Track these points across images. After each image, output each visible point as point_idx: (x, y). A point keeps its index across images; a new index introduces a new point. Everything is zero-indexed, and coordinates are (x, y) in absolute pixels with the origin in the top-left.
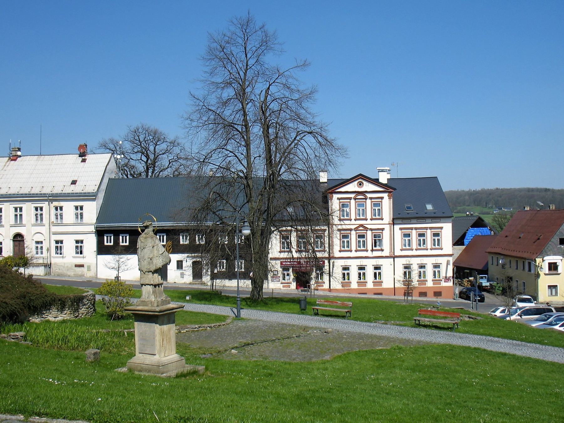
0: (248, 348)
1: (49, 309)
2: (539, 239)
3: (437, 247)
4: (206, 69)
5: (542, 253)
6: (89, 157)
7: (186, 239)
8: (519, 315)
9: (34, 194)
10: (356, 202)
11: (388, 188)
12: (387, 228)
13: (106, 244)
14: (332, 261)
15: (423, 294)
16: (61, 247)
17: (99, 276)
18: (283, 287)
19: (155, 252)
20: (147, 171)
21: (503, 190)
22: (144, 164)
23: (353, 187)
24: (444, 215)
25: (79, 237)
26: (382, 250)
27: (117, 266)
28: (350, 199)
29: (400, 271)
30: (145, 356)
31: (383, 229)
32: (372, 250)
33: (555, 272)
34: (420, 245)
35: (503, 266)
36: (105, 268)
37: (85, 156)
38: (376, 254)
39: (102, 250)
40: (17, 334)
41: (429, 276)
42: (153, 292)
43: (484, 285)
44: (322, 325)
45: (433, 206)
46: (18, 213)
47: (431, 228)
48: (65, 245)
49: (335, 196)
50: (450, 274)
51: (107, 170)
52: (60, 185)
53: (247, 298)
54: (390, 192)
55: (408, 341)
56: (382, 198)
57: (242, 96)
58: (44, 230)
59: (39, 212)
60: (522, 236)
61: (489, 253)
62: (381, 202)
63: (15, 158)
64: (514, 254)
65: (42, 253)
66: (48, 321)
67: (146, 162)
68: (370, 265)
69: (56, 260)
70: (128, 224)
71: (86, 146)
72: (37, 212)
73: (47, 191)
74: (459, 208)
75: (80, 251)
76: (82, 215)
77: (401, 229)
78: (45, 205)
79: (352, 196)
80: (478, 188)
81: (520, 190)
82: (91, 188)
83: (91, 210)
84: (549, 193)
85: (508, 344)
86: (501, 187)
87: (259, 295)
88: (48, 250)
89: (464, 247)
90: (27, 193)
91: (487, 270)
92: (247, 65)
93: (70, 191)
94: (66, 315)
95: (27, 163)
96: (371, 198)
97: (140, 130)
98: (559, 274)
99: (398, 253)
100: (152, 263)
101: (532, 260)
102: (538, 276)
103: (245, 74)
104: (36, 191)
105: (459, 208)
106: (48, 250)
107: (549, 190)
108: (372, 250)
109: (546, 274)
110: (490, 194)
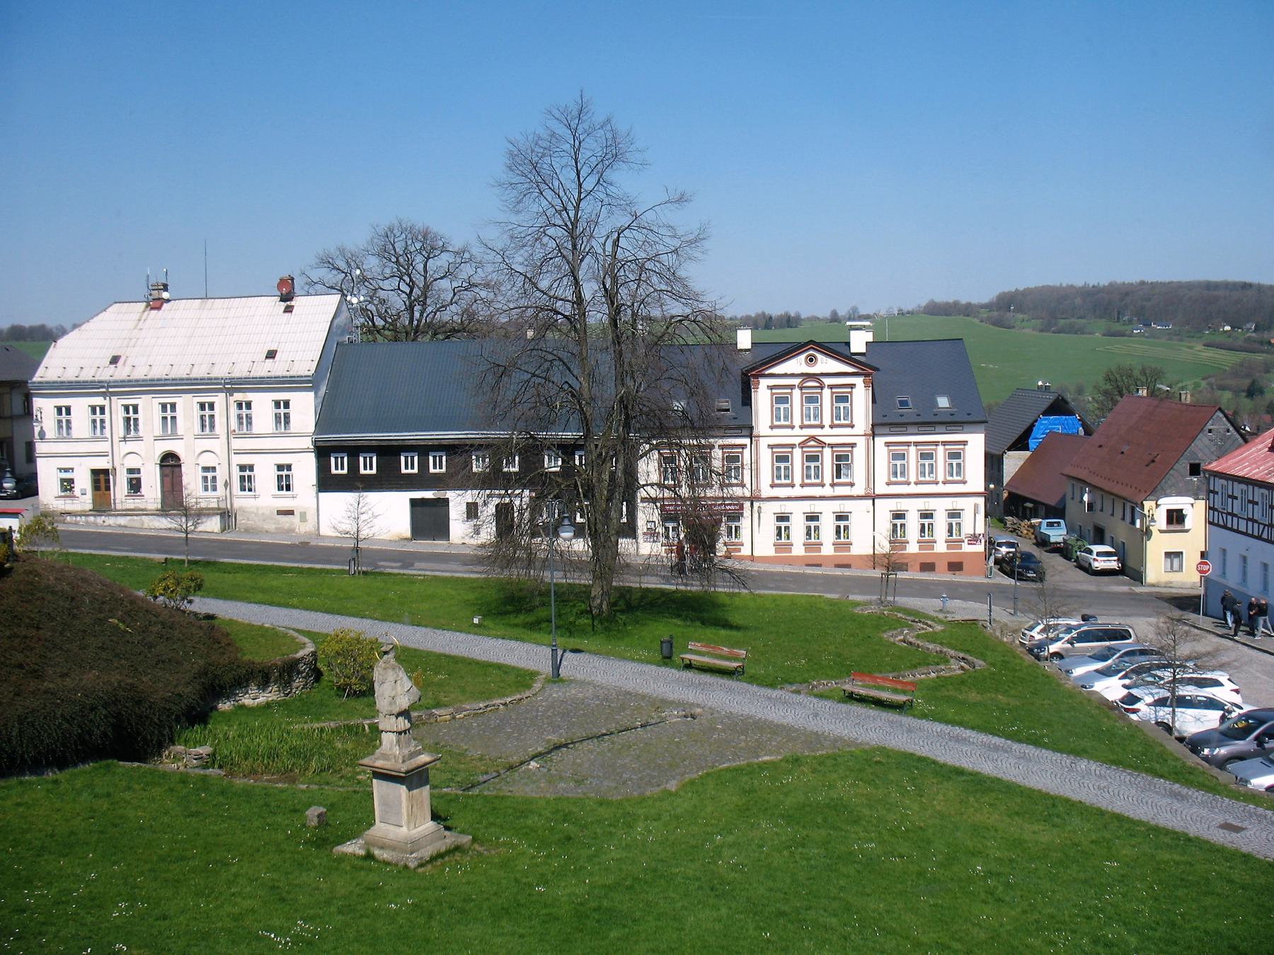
0: (556, 756)
5: (1155, 492)
6: (297, 302)
10: (802, 394)
11: (863, 365)
12: (861, 442)
13: (334, 471)
14: (756, 505)
15: (928, 567)
16: (250, 477)
17: (326, 531)
20: (411, 309)
23: (796, 365)
24: (970, 419)
25: (284, 460)
28: (792, 387)
29: (884, 524)
30: (388, 827)
31: (853, 445)
32: (833, 485)
33: (1178, 527)
36: (336, 516)
37: (291, 299)
38: (840, 491)
39: (327, 482)
42: (398, 741)
44: (691, 696)
45: (952, 401)
46: (169, 414)
49: (764, 383)
52: (247, 363)
54: (866, 375)
55: (816, 739)
56: (852, 386)
58: (218, 445)
59: (207, 412)
60: (1126, 448)
62: (851, 393)
63: (158, 303)
65: (214, 489)
66: (243, 707)
67: (409, 295)
68: (827, 511)
69: (242, 502)
71: (292, 279)
73: (221, 372)
74: (1062, 322)
75: (285, 484)
76: (287, 416)
77: (888, 444)
78: (219, 399)
79: (796, 381)
80: (1104, 282)
81: (1190, 286)
83: (304, 407)
85: (983, 744)
86: (1150, 278)
88: (227, 484)
89: (1028, 454)
91: (1064, 509)
93: (264, 373)
94: (271, 695)
95: (180, 312)
96: (831, 387)
98: (1187, 531)
99: (881, 488)
102: (1147, 533)
103: (577, 208)
105: (1062, 322)
106: (226, 484)
107: (1250, 285)
108: (833, 485)
109: (1161, 531)
110: (1127, 294)
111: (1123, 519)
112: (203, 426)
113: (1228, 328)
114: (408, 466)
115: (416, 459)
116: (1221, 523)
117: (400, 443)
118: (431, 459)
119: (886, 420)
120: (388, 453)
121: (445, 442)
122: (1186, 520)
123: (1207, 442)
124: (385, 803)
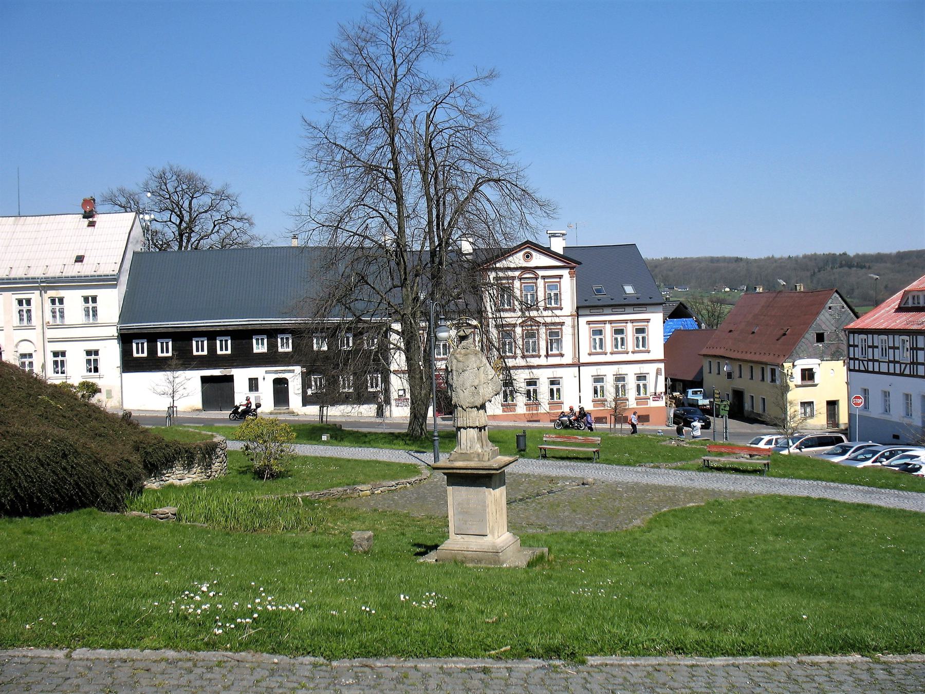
1: (172, 467)
2: (784, 334)
3: (641, 348)
4: (330, 81)
5: (791, 354)
6: (98, 219)
7: (263, 344)
8: (797, 447)
9: (28, 279)
11: (569, 259)
12: (568, 321)
13: (135, 355)
18: (504, 411)
19: (482, 376)
21: (674, 260)
22: (175, 229)
25: (92, 346)
26: (562, 355)
27: (171, 391)
28: (513, 278)
29: (588, 386)
31: (562, 324)
32: (547, 356)
33: (810, 383)
34: (616, 347)
35: (729, 375)
37: (92, 216)
38: (552, 360)
39: (129, 364)
40: (166, 510)
41: (632, 394)
43: (700, 403)
45: (635, 288)
46: (91, 305)
47: (632, 321)
48: (68, 358)
50: (661, 388)
51: (131, 240)
52: (58, 264)
53: (403, 434)
54: (571, 268)
56: (560, 277)
57: (390, 123)
61: (704, 355)
62: (559, 282)
64: (748, 357)
66: (172, 486)
67: (179, 226)
70: (186, 323)
71: (94, 200)
72: (21, 308)
73: (36, 272)
77: (589, 323)
78: (35, 296)
81: (699, 260)
82: (109, 267)
83: (110, 303)
84: (741, 264)
85: (855, 491)
86: (672, 255)
87: (422, 429)
90: (4, 276)
92: (396, 76)
93: (75, 274)
94: (194, 476)
96: (544, 277)
97: (169, 175)
100: (478, 393)
101: (778, 365)
102: (786, 389)
103: (393, 89)
104: (18, 273)
107: (741, 259)
108: (547, 356)
109: (797, 386)
110: (656, 267)
111: (763, 379)
112: (21, 320)
113: (727, 289)
114: (199, 348)
115: (205, 343)
116: (862, 368)
117: (193, 329)
118: (218, 343)
119: (587, 304)
120: (182, 338)
121: (230, 328)
122: (816, 376)
123: (828, 316)
124: (464, 512)
